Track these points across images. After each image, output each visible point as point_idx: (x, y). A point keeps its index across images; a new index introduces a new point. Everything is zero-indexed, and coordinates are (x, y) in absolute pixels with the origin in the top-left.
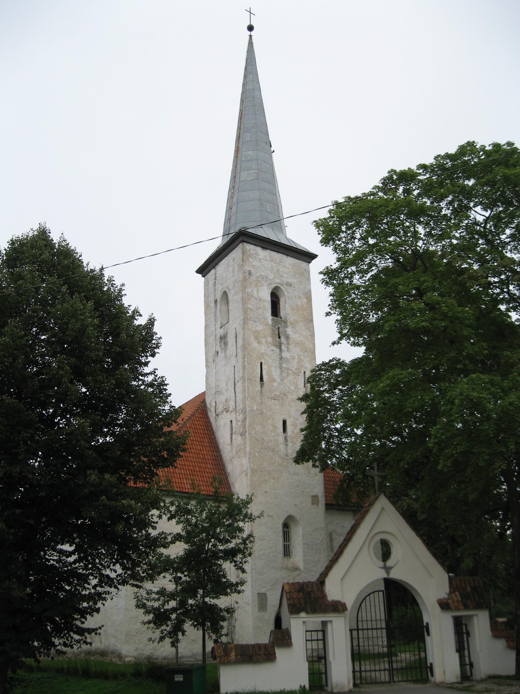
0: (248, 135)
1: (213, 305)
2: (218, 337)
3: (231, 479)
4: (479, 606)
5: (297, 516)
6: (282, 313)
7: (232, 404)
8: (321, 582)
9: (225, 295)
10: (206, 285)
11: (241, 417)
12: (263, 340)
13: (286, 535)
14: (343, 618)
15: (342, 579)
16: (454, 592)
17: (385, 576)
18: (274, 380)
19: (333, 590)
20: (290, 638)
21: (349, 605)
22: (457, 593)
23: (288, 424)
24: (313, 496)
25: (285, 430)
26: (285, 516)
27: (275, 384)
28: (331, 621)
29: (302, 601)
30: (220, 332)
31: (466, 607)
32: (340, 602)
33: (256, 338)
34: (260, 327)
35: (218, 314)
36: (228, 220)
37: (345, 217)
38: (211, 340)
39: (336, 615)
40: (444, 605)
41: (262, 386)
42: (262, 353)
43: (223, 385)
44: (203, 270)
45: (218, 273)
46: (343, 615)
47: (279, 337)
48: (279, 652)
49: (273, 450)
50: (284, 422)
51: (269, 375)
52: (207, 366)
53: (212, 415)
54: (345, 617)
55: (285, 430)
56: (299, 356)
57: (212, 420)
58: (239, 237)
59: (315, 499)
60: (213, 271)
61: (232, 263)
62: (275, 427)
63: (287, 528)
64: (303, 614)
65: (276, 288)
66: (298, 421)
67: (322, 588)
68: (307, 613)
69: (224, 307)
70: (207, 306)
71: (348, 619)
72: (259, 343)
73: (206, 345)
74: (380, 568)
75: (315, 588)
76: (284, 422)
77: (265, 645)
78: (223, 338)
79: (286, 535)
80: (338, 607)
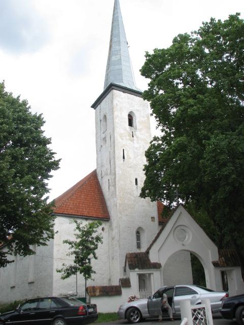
0: (116, 38)
1: (99, 123)
2: (102, 138)
3: (109, 209)
4: (235, 265)
5: (144, 228)
6: (134, 124)
7: (109, 171)
8: (148, 252)
9: (105, 117)
10: (96, 113)
11: (113, 177)
12: (124, 138)
13: (138, 238)
14: (159, 272)
15: (159, 251)
16: (221, 257)
17: (181, 248)
18: (130, 158)
19: (153, 258)
20: (130, 283)
21: (163, 265)
22: (223, 258)
23: (138, 180)
24: (152, 218)
25: (136, 184)
26: (138, 227)
27: (131, 160)
28: (153, 273)
29: (136, 263)
30: (103, 136)
31: (228, 265)
32: (157, 263)
33: (121, 137)
34: (122, 131)
35: (102, 126)
36: (107, 80)
37: (154, 65)
38: (99, 141)
39: (155, 270)
40: (216, 264)
41: (124, 161)
42: (124, 145)
43: (105, 162)
44: (94, 106)
45: (102, 108)
46: (159, 270)
47: (133, 137)
48: (124, 290)
49: (130, 194)
50: (136, 180)
51: (128, 156)
52: (97, 154)
53: (99, 178)
54: (160, 271)
55: (136, 184)
56: (143, 146)
57: (100, 180)
58: (110, 87)
59: (153, 218)
60: (99, 106)
61: (108, 100)
62: (131, 182)
63: (139, 233)
64: (137, 270)
65: (131, 112)
66: (142, 178)
67: (148, 255)
68: (139, 269)
69: (104, 123)
70: (96, 123)
71: (162, 272)
72: (122, 139)
73: (96, 143)
74: (19, 96)
75: (144, 256)
76: (136, 180)
77: (116, 287)
78: (105, 139)
79: (138, 238)
80: (157, 266)
